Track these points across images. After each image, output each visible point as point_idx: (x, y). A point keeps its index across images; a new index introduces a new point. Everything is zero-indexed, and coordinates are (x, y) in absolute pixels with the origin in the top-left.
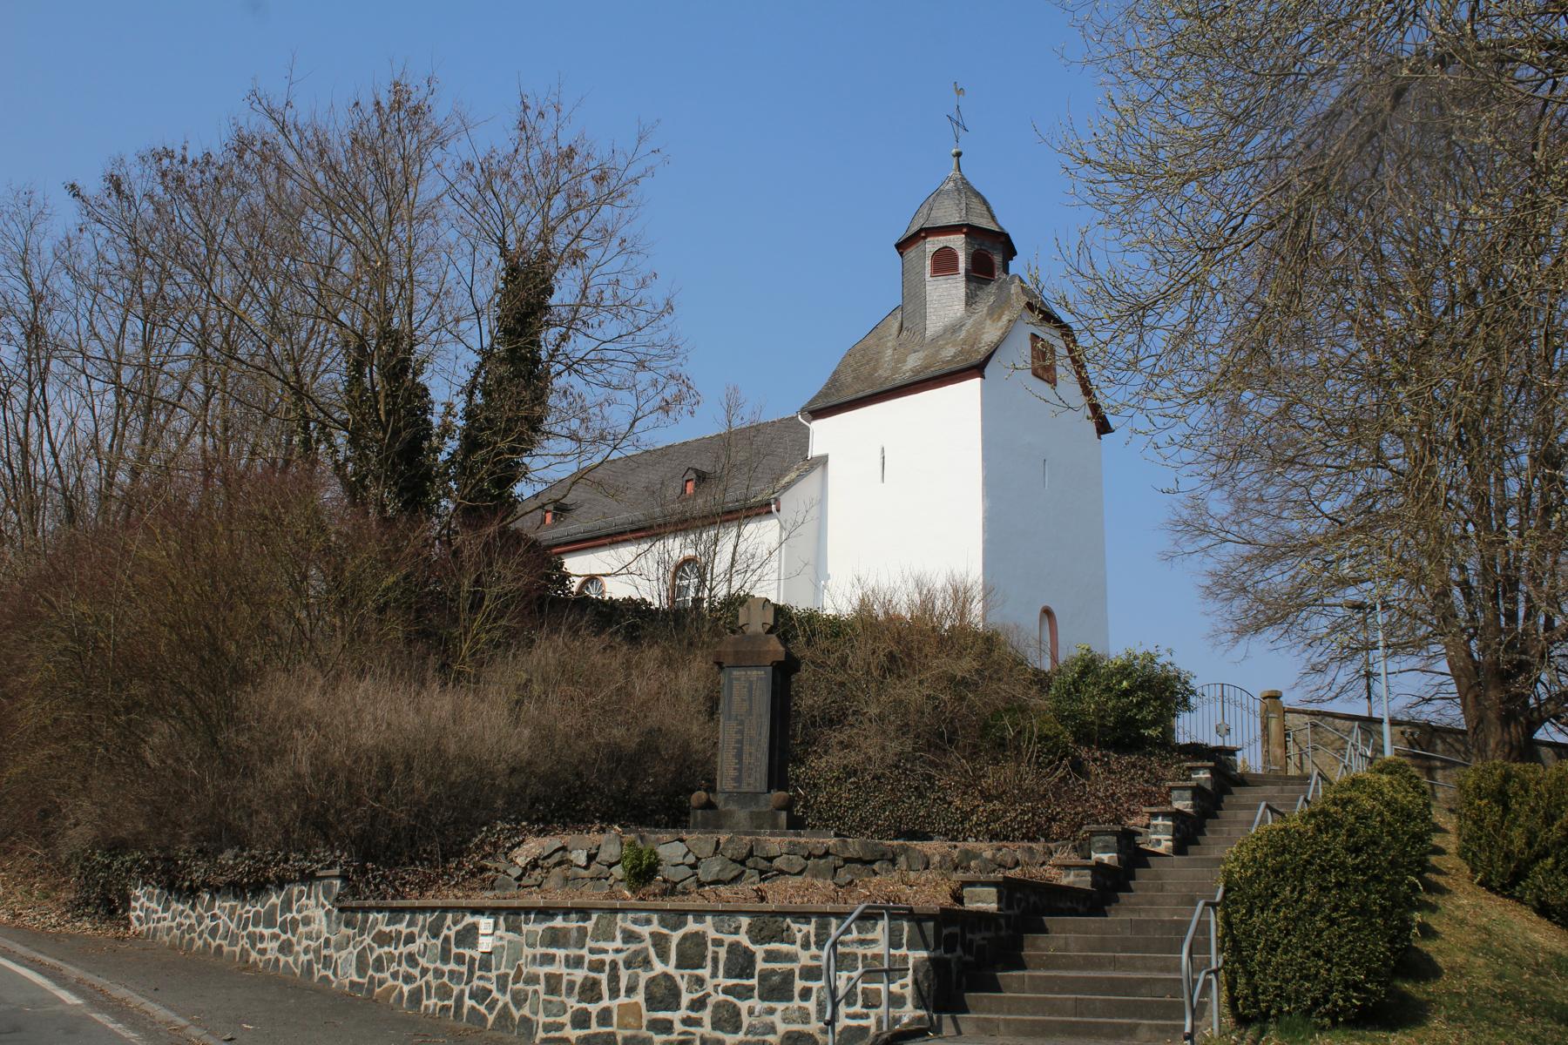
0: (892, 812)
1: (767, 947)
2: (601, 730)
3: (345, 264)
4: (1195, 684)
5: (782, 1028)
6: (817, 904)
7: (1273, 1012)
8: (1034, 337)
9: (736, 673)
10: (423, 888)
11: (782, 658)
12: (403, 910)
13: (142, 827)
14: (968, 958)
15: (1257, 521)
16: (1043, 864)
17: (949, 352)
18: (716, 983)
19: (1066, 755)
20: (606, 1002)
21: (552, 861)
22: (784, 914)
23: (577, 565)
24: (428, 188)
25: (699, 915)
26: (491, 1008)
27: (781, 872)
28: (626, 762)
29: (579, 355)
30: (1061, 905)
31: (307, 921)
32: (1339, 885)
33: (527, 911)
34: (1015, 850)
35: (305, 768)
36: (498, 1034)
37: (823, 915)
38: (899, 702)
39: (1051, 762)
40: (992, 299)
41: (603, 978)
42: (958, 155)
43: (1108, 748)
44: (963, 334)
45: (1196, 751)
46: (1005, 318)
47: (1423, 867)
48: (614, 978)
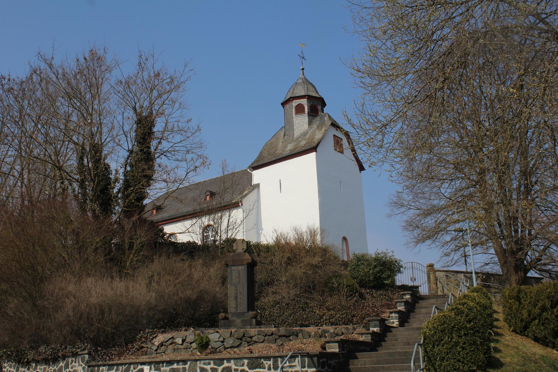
0: (293, 317)
2: (182, 292)
3: (74, 118)
6: (271, 353)
8: (334, 135)
9: (233, 268)
10: (120, 355)
11: (250, 261)
12: (113, 365)
13: (7, 339)
14: (330, 370)
15: (421, 201)
17: (303, 143)
19: (357, 292)
21: (168, 343)
22: (261, 358)
23: (168, 229)
24: (105, 88)
25: (229, 360)
27: (256, 342)
28: (193, 304)
29: (165, 149)
30: (361, 348)
32: (465, 335)
33: (163, 362)
34: (342, 328)
35: (71, 313)
37: (275, 357)
38: (293, 275)
39: (351, 295)
40: (318, 122)
42: (303, 69)
43: (372, 289)
44: (308, 136)
45: (404, 288)
46: (323, 130)
47: (492, 326)
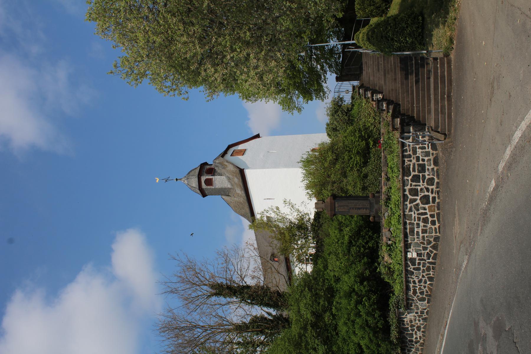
5: (432, 166)
8: (231, 155)
9: (336, 211)
18: (422, 185)
20: (428, 216)
31: (411, 321)
37: (403, 156)
44: (231, 176)
46: (226, 164)
48: (422, 214)
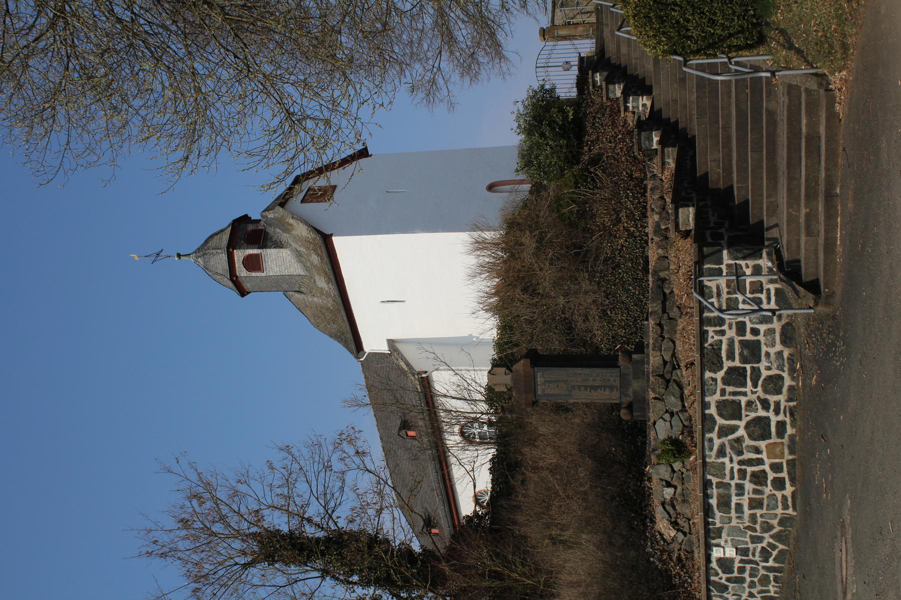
1: (724, 359)
2: (582, 485)
4: (536, 86)
5: (779, 347)
6: (693, 328)
7: (755, 21)
8: (302, 202)
9: (539, 392)
14: (727, 225)
15: (425, 47)
16: (661, 180)
17: (315, 259)
18: (750, 392)
19: (587, 169)
22: (702, 348)
23: (467, 507)
25: (705, 405)
26: (774, 547)
27: (674, 355)
29: (322, 510)
33: (706, 524)
34: (652, 199)
36: (791, 541)
37: (702, 322)
39: (593, 179)
40: (278, 230)
41: (750, 470)
42: (179, 255)
44: (303, 249)
45: (582, 83)
46: (291, 221)
48: (750, 462)
